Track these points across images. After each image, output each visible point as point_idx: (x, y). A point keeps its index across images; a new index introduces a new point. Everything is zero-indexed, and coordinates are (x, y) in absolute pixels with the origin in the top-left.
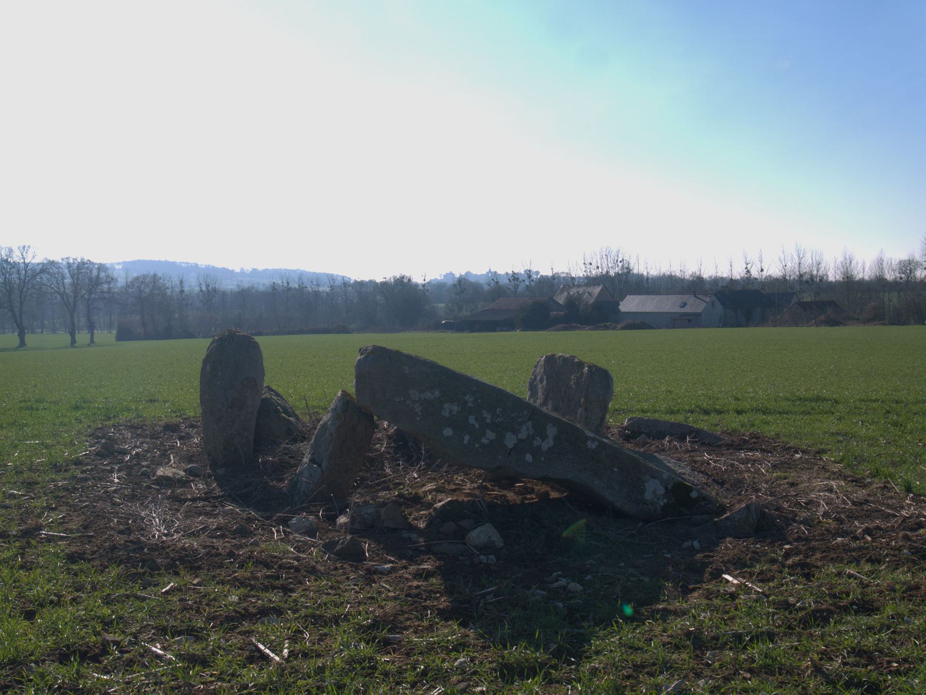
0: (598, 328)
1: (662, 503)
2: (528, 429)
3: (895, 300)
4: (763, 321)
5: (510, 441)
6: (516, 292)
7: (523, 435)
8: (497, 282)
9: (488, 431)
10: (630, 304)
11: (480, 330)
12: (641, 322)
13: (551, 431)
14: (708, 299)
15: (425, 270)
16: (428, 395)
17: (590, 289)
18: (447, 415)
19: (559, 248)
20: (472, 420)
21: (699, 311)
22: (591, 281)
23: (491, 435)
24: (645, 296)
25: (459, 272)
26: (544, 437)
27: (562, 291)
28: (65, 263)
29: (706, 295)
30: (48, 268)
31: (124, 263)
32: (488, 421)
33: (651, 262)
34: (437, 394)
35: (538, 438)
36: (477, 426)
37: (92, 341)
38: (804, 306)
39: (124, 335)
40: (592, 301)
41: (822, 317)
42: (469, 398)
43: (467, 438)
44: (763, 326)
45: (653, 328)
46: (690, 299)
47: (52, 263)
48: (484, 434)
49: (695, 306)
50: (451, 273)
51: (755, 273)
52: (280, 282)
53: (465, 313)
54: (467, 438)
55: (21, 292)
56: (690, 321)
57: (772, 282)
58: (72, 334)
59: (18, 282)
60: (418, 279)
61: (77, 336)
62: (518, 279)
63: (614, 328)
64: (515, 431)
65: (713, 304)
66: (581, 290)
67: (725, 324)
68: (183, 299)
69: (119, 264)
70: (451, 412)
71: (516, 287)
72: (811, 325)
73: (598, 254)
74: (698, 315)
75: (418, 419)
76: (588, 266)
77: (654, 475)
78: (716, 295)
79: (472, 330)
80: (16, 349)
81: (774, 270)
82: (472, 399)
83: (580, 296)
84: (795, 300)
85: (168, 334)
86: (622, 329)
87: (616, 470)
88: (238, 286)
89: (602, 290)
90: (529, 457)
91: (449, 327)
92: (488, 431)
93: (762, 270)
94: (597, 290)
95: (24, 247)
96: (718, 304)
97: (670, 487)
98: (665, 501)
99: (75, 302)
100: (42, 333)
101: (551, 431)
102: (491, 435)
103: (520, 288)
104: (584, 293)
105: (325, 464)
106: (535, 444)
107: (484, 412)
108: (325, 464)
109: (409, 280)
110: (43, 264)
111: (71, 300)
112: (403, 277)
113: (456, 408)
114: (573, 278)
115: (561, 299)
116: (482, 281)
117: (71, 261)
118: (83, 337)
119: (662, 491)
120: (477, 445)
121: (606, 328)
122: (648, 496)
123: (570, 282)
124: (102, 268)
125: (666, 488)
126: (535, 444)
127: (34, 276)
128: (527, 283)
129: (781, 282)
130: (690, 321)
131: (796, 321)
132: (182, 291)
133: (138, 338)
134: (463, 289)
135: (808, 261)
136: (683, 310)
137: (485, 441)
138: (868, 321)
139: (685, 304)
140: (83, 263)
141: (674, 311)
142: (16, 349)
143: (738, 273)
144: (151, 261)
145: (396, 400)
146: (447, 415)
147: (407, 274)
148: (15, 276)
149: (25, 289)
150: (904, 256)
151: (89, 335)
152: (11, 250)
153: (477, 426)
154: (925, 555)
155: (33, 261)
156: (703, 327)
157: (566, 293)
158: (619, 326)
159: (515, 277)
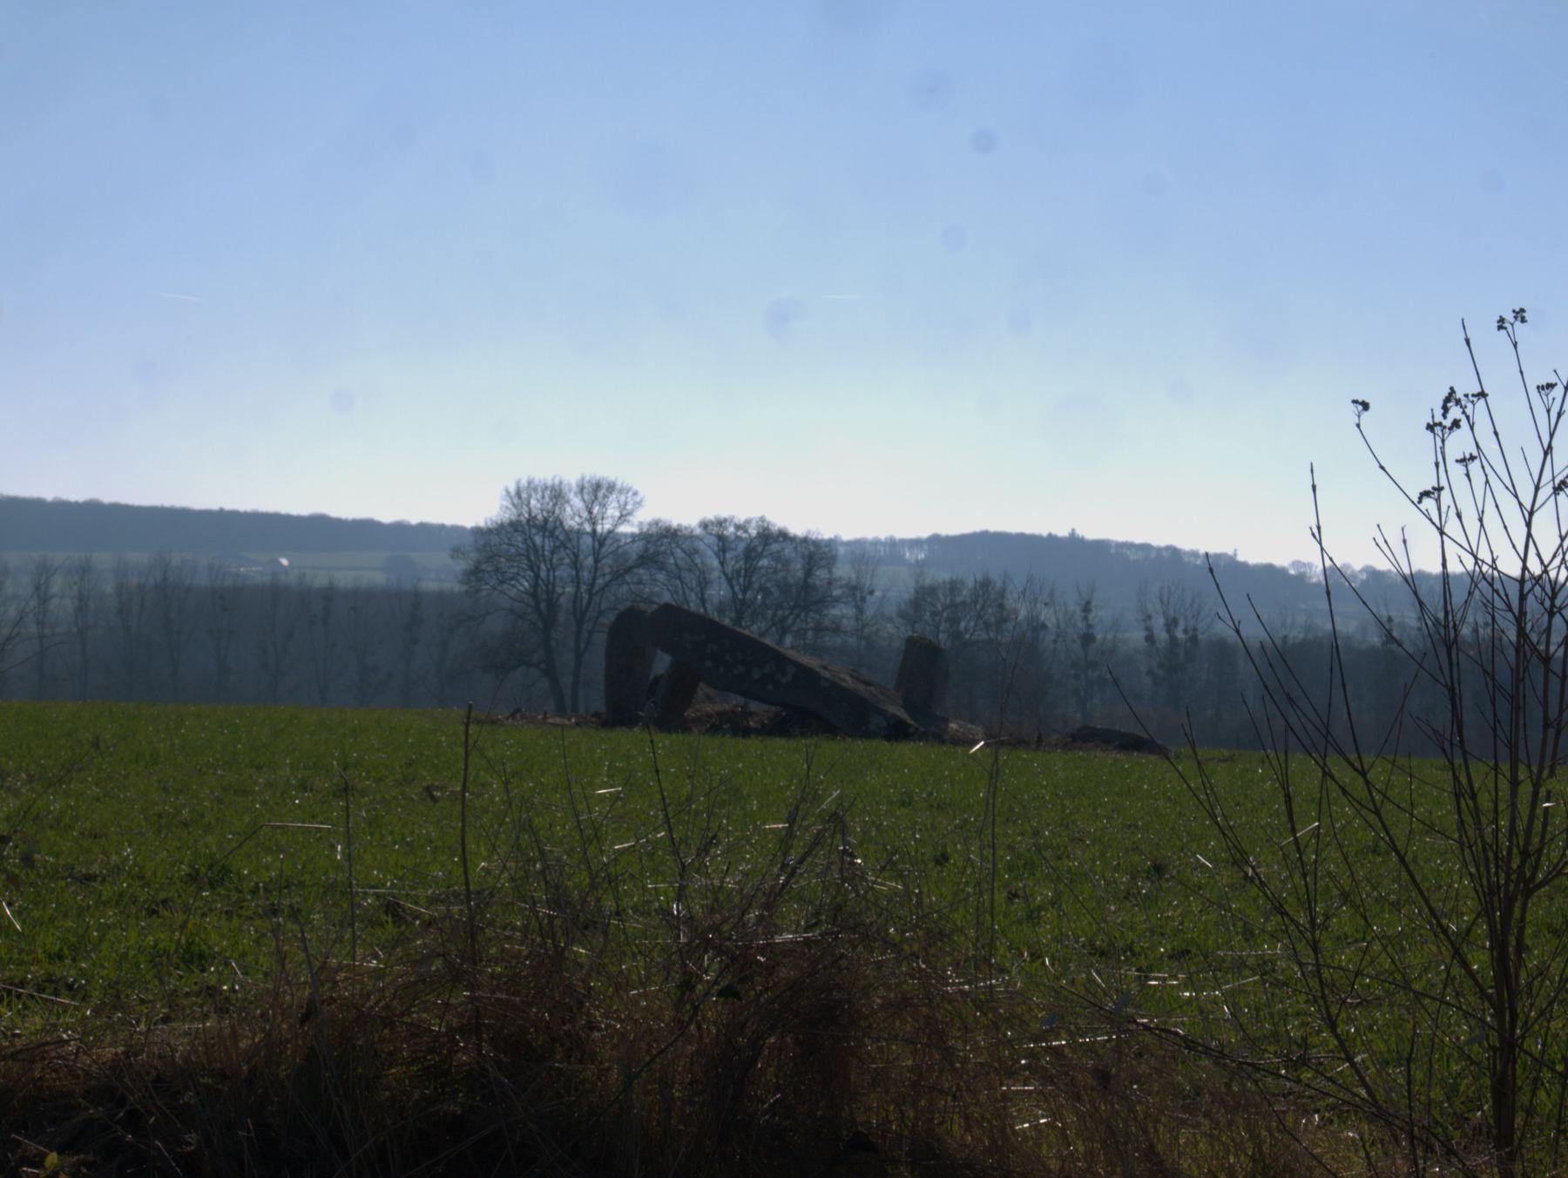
5: (756, 674)
30: (662, 544)
31: (935, 540)
43: (722, 669)
90: (770, 687)
132: (1088, 639)
148: (564, 572)
155: (624, 529)
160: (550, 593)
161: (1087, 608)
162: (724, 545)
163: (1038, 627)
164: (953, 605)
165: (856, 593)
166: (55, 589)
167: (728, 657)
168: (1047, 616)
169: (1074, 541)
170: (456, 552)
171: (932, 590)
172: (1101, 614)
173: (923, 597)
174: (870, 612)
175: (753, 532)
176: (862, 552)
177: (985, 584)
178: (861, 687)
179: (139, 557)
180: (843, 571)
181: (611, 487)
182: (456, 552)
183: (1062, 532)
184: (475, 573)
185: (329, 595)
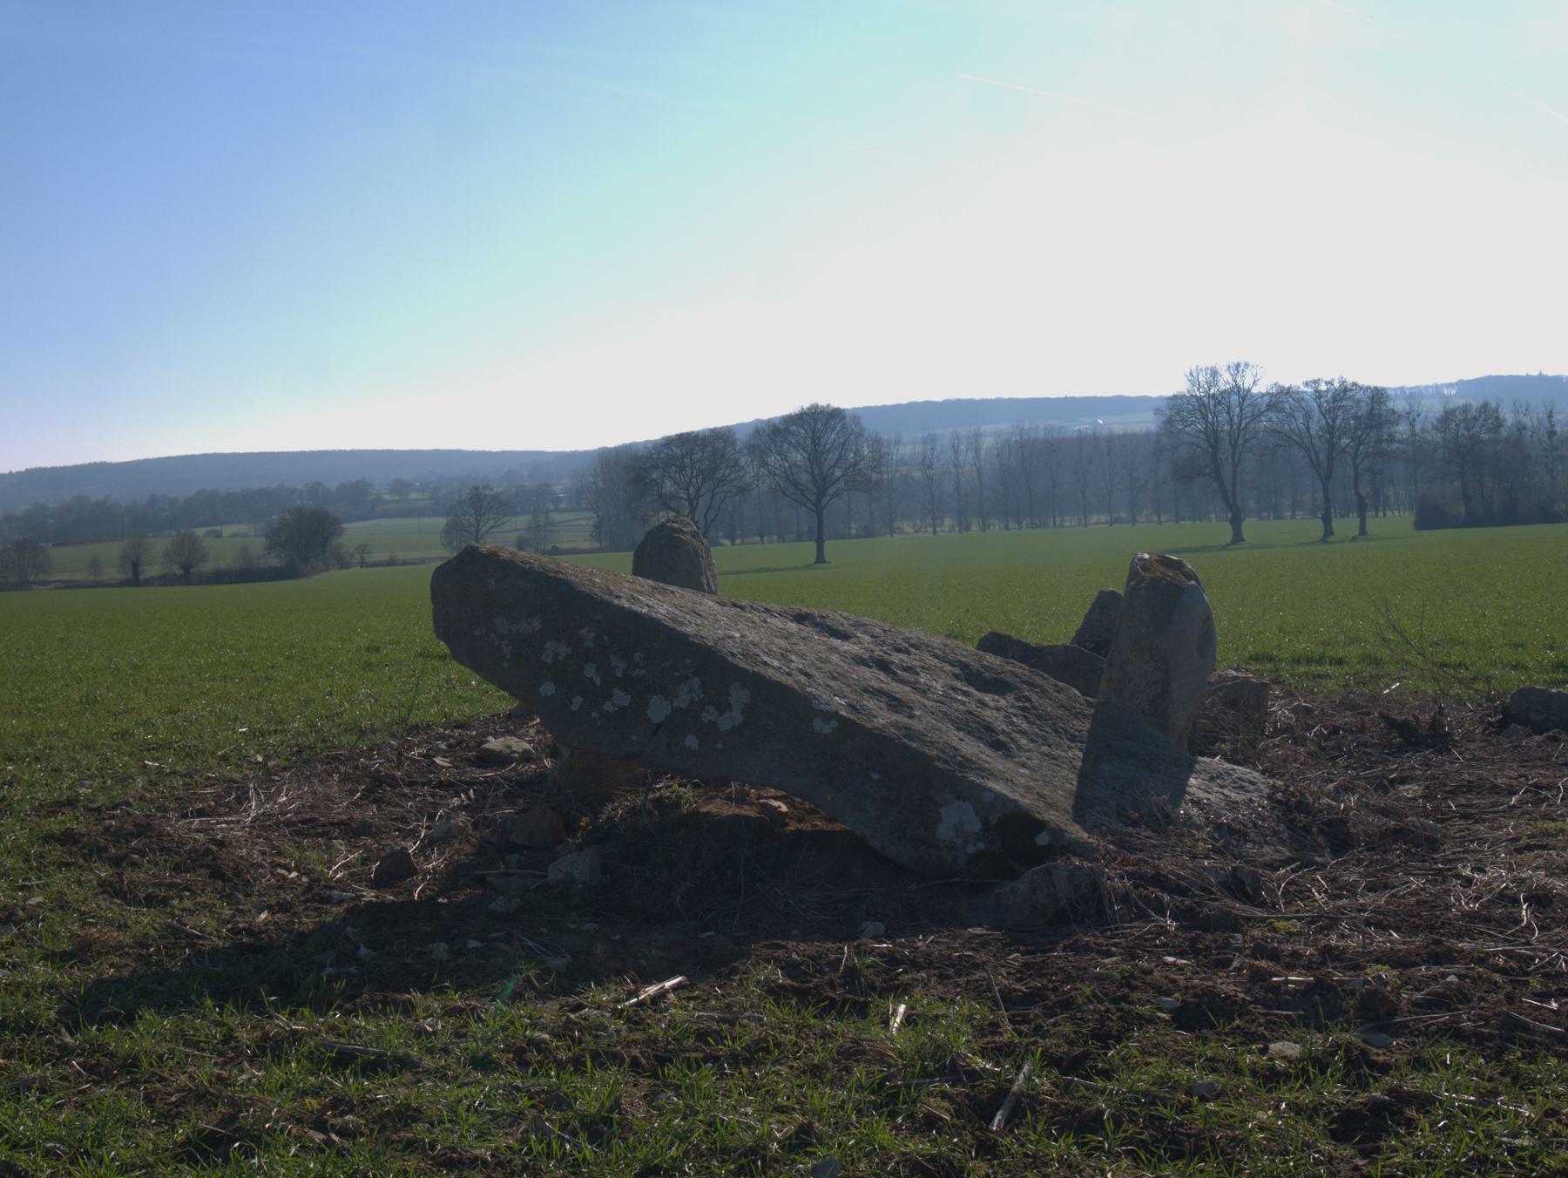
1: (971, 850)
2: (691, 690)
5: (658, 710)
7: (682, 701)
9: (616, 691)
13: (739, 696)
18: (549, 661)
20: (590, 671)
23: (621, 698)
26: (724, 706)
28: (1310, 390)
30: (1280, 399)
31: (1460, 382)
32: (619, 673)
34: (537, 624)
35: (712, 708)
36: (598, 682)
37: (1363, 531)
39: (1430, 517)
42: (588, 634)
43: (578, 701)
47: (1288, 392)
48: (610, 697)
54: (578, 701)
55: (1234, 446)
58: (1327, 520)
59: (1226, 427)
61: (1337, 523)
68: (1556, 448)
69: (1450, 385)
70: (556, 655)
80: (1224, 547)
82: (592, 635)
85: (1510, 515)
87: (875, 776)
90: (691, 741)
92: (616, 691)
95: (1238, 366)
97: (993, 819)
98: (981, 845)
99: (1330, 459)
100: (1293, 517)
101: (739, 696)
102: (621, 698)
106: (706, 717)
107: (612, 658)
110: (1272, 395)
111: (1322, 457)
117: (1323, 387)
118: (1346, 525)
119: (975, 825)
120: (594, 715)
122: (944, 832)
124: (1378, 395)
125: (986, 822)
127: (1256, 417)
132: (1552, 433)
133: (1455, 523)
137: (608, 707)
140: (1345, 390)
142: (1224, 547)
144: (1511, 377)
145: (477, 633)
148: (1224, 417)
149: (1240, 442)
151: (1357, 522)
152: (1214, 373)
153: (598, 682)
154: (6, 918)
155: (1255, 390)
160: (1215, 432)
161: (1550, 416)
162: (1318, 394)
163: (1521, 428)
164: (1465, 420)
165: (1410, 417)
166: (962, 447)
167: (590, 671)
168: (1526, 421)
169: (1542, 379)
170: (1158, 411)
171: (1453, 411)
172: (1558, 417)
173: (1447, 417)
174: (1418, 428)
175: (1337, 385)
176: (1413, 395)
177: (1485, 406)
178: (1039, 681)
179: (1005, 427)
180: (1400, 406)
181: (1247, 365)
182: (1158, 411)
183: (1535, 373)
184: (1170, 421)
185: (1111, 439)
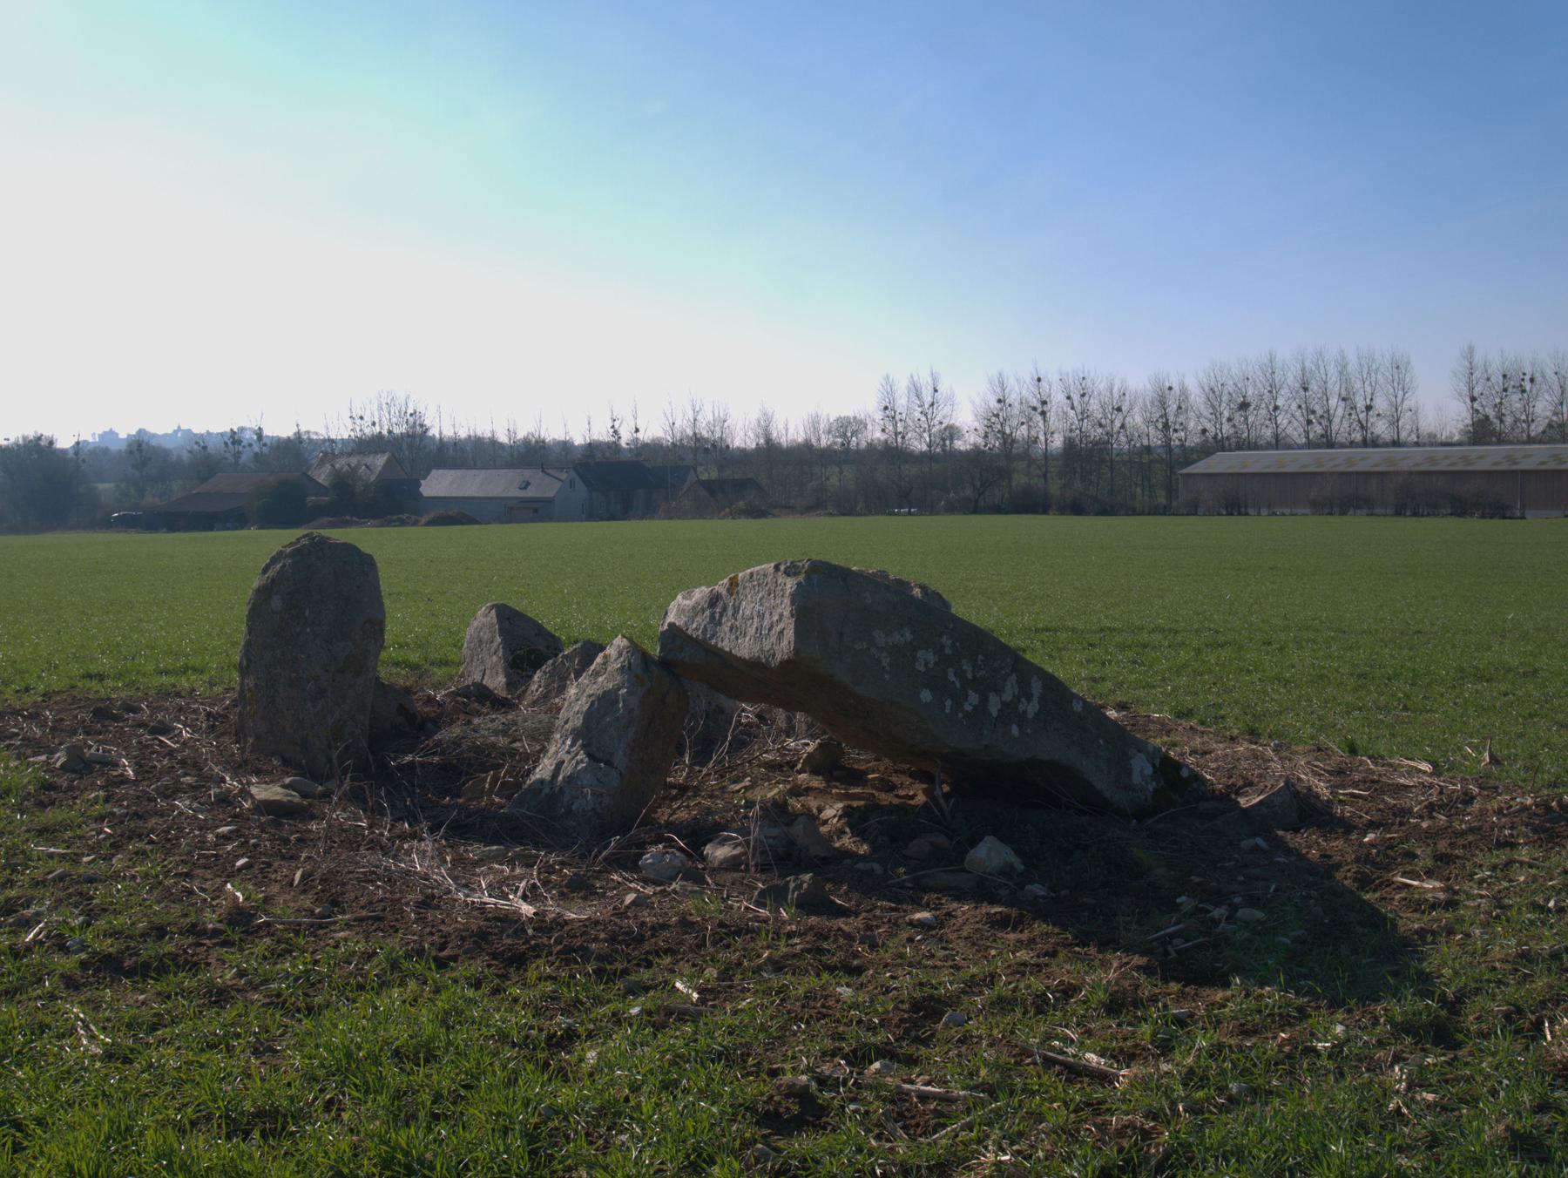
0: (388, 524)
3: (834, 480)
4: (649, 511)
6: (237, 463)
7: (1007, 696)
8: (205, 448)
9: (970, 692)
10: (437, 484)
11: (187, 529)
12: (456, 514)
14: (564, 476)
15: (71, 425)
16: (897, 638)
17: (369, 460)
18: (922, 669)
19: (308, 390)
21: (550, 494)
22: (368, 445)
24: (459, 472)
25: (126, 429)
26: (1029, 698)
27: (322, 462)
29: (561, 469)
32: (970, 676)
33: (451, 419)
38: (709, 486)
40: (373, 478)
41: (741, 504)
42: (946, 641)
43: (949, 703)
44: (652, 518)
45: (476, 522)
46: (534, 476)
49: (543, 486)
50: (111, 432)
51: (626, 437)
52: (91, 440)
53: (150, 500)
56: (536, 511)
57: (655, 448)
60: (64, 442)
62: (240, 442)
63: (415, 523)
64: (999, 690)
65: (572, 483)
66: (354, 461)
67: (591, 516)
71: (238, 455)
72: (724, 517)
73: (375, 401)
74: (549, 501)
75: (887, 676)
76: (358, 421)
77: (1141, 747)
78: (575, 469)
79: (172, 528)
81: (654, 428)
83: (354, 470)
84: (692, 477)
86: (429, 524)
88: (995, 421)
89: (388, 461)
90: (1015, 730)
91: (129, 523)
93: (637, 430)
94: (380, 461)
96: (580, 485)
101: (1036, 687)
103: (244, 458)
104: (359, 465)
105: (620, 759)
107: (964, 662)
108: (620, 759)
109: (51, 443)
112: (39, 438)
113: (932, 658)
114: (333, 441)
115: (322, 476)
116: (168, 445)
119: (1149, 771)
121: (402, 523)
122: (1136, 779)
123: (329, 450)
126: (1022, 708)
128: (257, 449)
129: (676, 449)
130: (536, 511)
131: (700, 512)
134: (142, 454)
135: (706, 418)
136: (524, 494)
138: (808, 510)
139: (528, 484)
141: (510, 494)
143: (601, 433)
146: (922, 669)
147: (47, 432)
150: (848, 411)
156: (559, 520)
157: (328, 466)
158: (423, 521)
159: (234, 438)
